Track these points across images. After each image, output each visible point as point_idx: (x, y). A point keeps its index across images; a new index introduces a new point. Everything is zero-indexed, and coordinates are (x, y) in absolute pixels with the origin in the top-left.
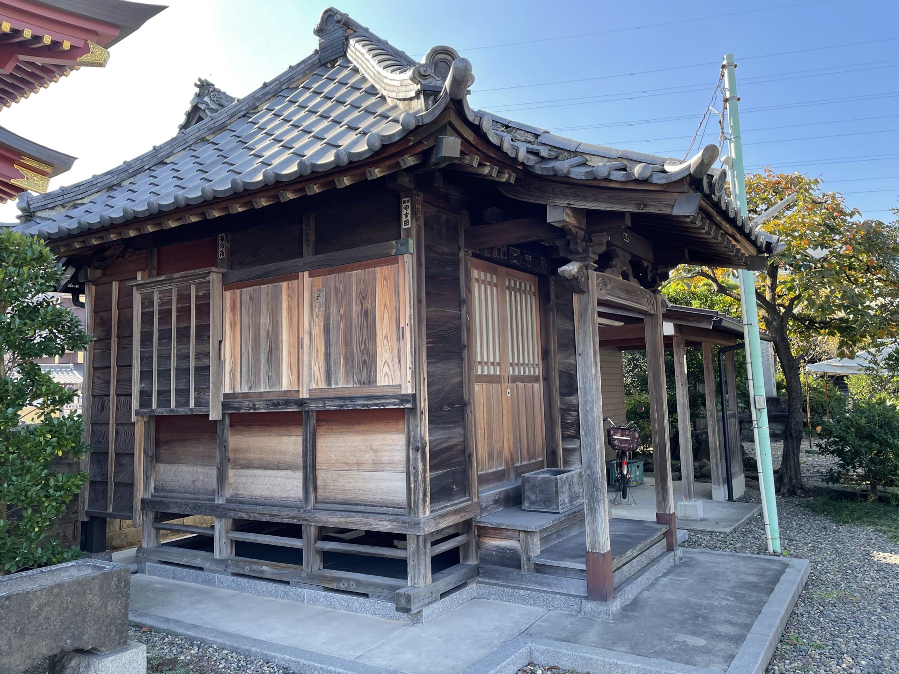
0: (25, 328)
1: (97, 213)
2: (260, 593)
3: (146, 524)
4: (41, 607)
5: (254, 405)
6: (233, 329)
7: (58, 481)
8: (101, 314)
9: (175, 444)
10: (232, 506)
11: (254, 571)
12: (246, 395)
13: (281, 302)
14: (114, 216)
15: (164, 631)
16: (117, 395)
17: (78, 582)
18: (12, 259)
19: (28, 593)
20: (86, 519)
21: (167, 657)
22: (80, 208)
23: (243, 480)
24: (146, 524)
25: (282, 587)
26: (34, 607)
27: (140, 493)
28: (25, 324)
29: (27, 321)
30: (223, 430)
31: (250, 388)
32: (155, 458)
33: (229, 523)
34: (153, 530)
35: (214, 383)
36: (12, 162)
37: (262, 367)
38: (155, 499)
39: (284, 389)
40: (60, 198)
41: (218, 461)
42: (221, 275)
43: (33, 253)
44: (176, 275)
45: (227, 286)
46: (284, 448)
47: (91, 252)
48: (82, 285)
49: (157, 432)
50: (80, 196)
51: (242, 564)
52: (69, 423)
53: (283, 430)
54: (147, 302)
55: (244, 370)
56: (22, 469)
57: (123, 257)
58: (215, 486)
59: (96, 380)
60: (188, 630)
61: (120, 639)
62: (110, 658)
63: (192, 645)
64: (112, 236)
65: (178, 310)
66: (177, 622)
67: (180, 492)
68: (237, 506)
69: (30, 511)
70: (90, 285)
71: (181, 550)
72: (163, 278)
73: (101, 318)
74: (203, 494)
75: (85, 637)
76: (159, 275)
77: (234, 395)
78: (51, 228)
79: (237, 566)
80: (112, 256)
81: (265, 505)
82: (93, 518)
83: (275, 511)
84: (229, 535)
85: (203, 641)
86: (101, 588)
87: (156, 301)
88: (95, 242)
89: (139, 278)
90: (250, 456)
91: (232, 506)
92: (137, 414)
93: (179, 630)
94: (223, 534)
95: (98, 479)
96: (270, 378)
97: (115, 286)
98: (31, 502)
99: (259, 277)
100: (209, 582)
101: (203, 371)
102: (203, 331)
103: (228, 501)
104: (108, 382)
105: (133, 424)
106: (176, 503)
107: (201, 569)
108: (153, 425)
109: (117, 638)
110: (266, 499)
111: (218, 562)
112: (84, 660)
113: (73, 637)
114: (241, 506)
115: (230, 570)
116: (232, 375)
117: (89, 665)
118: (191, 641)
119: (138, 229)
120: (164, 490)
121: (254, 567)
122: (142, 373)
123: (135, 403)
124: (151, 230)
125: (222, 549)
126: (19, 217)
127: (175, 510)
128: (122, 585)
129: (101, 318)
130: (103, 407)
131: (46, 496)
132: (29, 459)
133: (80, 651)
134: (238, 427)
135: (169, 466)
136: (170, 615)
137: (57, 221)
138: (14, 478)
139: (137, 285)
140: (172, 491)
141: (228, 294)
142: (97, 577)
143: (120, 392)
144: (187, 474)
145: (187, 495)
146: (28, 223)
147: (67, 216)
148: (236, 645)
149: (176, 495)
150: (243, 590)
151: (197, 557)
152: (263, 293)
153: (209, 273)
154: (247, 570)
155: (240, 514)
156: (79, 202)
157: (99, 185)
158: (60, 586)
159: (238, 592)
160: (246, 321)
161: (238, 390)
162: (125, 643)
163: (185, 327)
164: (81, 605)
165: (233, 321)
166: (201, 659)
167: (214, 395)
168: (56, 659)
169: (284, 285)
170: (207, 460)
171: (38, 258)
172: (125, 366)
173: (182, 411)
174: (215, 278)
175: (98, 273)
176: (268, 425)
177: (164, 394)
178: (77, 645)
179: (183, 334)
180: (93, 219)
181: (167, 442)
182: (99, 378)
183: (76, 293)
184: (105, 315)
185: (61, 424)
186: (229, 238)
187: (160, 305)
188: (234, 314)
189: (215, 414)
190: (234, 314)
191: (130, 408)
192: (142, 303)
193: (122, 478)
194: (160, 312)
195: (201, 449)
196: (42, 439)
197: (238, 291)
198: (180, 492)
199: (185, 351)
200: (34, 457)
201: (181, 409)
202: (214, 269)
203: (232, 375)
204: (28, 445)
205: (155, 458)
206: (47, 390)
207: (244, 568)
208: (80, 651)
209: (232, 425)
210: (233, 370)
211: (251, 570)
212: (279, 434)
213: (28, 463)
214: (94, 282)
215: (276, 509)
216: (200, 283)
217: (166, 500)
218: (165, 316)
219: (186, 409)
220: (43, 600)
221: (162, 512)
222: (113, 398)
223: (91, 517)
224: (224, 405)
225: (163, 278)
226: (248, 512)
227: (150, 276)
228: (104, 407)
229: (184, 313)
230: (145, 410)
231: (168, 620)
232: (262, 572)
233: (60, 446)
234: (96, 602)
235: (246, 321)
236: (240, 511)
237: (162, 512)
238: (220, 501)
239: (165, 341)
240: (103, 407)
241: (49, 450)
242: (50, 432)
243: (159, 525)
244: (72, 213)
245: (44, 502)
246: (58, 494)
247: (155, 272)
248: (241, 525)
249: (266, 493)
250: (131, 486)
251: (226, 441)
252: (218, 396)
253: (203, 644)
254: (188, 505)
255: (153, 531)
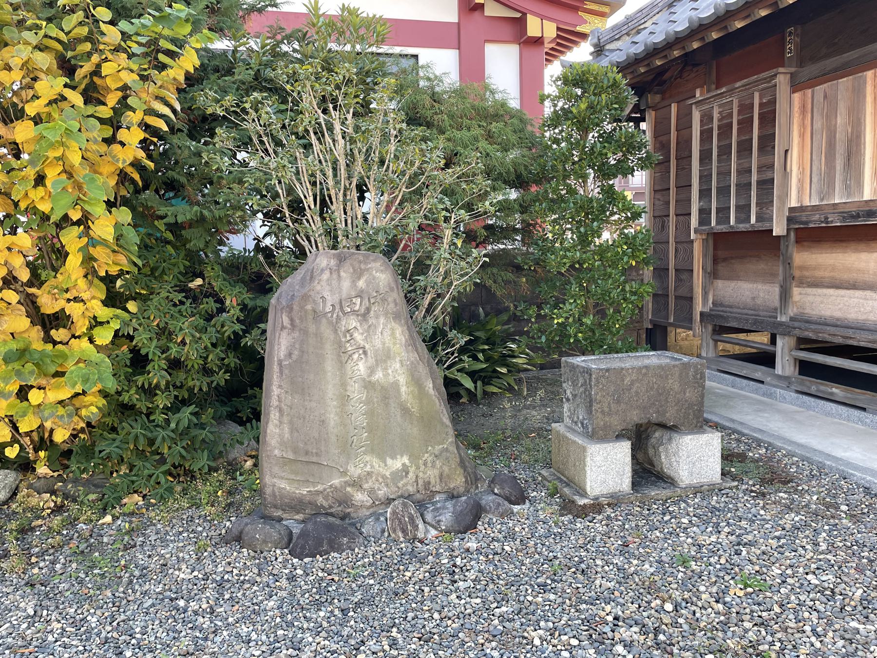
0: (605, 151)
1: (661, 32)
2: (828, 414)
3: (704, 336)
4: (632, 383)
5: (826, 218)
6: (802, 136)
7: (632, 287)
8: (660, 138)
9: (733, 261)
10: (796, 324)
11: (818, 390)
12: (815, 208)
13: (865, 97)
14: (679, 29)
15: (730, 428)
16: (676, 215)
17: (660, 367)
18: (592, 88)
19: (622, 369)
20: (650, 327)
21: (736, 451)
22: (643, 32)
23: (810, 298)
24: (704, 336)
25: (857, 413)
26: (627, 381)
27: (699, 307)
28: (605, 147)
29: (606, 145)
30: (787, 246)
31: (822, 200)
32: (713, 275)
33: (792, 342)
34: (711, 341)
35: (779, 197)
36: (576, 9)
37: (837, 176)
38: (713, 313)
39: (865, 198)
40: (626, 27)
41: (781, 278)
42: (788, 76)
43: (609, 81)
44: (738, 84)
45: (796, 86)
46: (862, 265)
47: (652, 77)
48: (642, 112)
49: (715, 248)
50: (643, 21)
51: (808, 383)
52: (640, 236)
53: (862, 246)
54: (707, 118)
55: (815, 180)
56: (605, 275)
57: (680, 77)
58: (777, 303)
59: (657, 202)
60: (755, 432)
61: (698, 422)
62: (690, 437)
63: (760, 446)
64: (675, 52)
65: (739, 123)
66: (741, 423)
67: (739, 308)
68: (803, 325)
69: (611, 311)
70: (651, 111)
71: (740, 363)
72: (724, 90)
73: (661, 143)
74: (763, 311)
75: (668, 415)
76: (717, 88)
77: (802, 209)
78: (620, 57)
79: (802, 383)
80: (671, 78)
81: (837, 326)
82: (656, 326)
83: (850, 333)
84: (793, 353)
85: (770, 444)
86: (680, 375)
87: (716, 116)
88: (659, 63)
89: (698, 95)
90: (819, 274)
91: (796, 324)
92: (696, 231)
93: (746, 431)
94: (786, 351)
95: (660, 293)
96: (847, 188)
97: (674, 108)
98: (613, 303)
99: (836, 70)
100: (771, 396)
101: (766, 185)
102: (767, 142)
103: (792, 319)
104: (668, 203)
105: (692, 241)
106: (735, 318)
107: (762, 382)
108: (711, 242)
109: (695, 421)
110: (838, 319)
111: (780, 377)
112: (667, 434)
113: (658, 412)
114: (807, 325)
115: (793, 387)
116: (799, 185)
117: (670, 439)
118: (759, 443)
119: (703, 39)
120: (722, 305)
121: (822, 388)
122: (701, 191)
123: (694, 222)
124: (715, 37)
125: (785, 365)
126: (591, 54)
127: (734, 324)
128: (699, 376)
129: (661, 143)
130: (663, 227)
131: (624, 299)
132: (610, 266)
133: (663, 426)
134: (805, 244)
135: (727, 283)
136: (735, 417)
137: (624, 49)
138: (600, 282)
139: (695, 103)
140: (731, 307)
141: (797, 96)
142: (677, 366)
143: (679, 212)
144: (748, 290)
145: (746, 311)
146: (599, 58)
147: (633, 42)
148: (808, 455)
149: (735, 310)
150: (809, 408)
151: (759, 372)
152: (841, 87)
153: (775, 75)
154: (813, 389)
155: (807, 333)
156: (642, 27)
157: (660, 5)
158: (646, 367)
159: (801, 409)
160: (818, 125)
161: (807, 203)
162: (701, 427)
163: (746, 140)
164: (664, 387)
165: (803, 125)
166: (770, 459)
167: (779, 209)
168: (642, 429)
169: (870, 74)
170: (768, 277)
171: (612, 85)
172: (684, 187)
173: (742, 227)
174: (782, 81)
175: (658, 97)
176: (842, 241)
177: (723, 211)
178: (660, 419)
179: (745, 148)
180: (659, 38)
181: (725, 260)
182: (659, 200)
183: (637, 122)
184: (663, 139)
185: (634, 237)
186: (799, 31)
187: (719, 120)
188: (803, 119)
189: (779, 229)
190: (803, 119)
191: (689, 227)
192: (701, 121)
193: (683, 292)
194: (719, 128)
195: (762, 266)
196: (619, 250)
197: (809, 92)
198: (739, 308)
199: (746, 165)
200: (614, 265)
201: (741, 226)
202: (781, 70)
203: (799, 185)
204: (609, 254)
205: (713, 275)
206: (623, 206)
207: (809, 388)
208: (663, 426)
209: (798, 241)
210: (801, 181)
211: (818, 390)
212: (857, 251)
213: (609, 270)
214: (655, 108)
215: (851, 331)
216: (763, 89)
217: (725, 315)
218: (725, 130)
219: (747, 225)
220: (634, 377)
221: (721, 326)
222: (672, 218)
223: (655, 325)
224: (790, 220)
225: (724, 90)
226: (815, 332)
227: (709, 91)
228: (664, 227)
229: (746, 125)
230: (704, 228)
231: (733, 421)
232: (832, 394)
233: (633, 257)
234: (676, 387)
235: (818, 125)
236: (806, 330)
237: (721, 326)
238: (782, 319)
239: (725, 157)
240: (663, 227)
241: (625, 259)
242: (626, 243)
243: (717, 337)
244: (637, 39)
245: (622, 304)
246: (633, 298)
247: (714, 86)
248: (804, 343)
249: (838, 314)
250: (690, 299)
251: (791, 258)
252: (783, 211)
253: (769, 446)
254: (747, 320)
255: (711, 343)
